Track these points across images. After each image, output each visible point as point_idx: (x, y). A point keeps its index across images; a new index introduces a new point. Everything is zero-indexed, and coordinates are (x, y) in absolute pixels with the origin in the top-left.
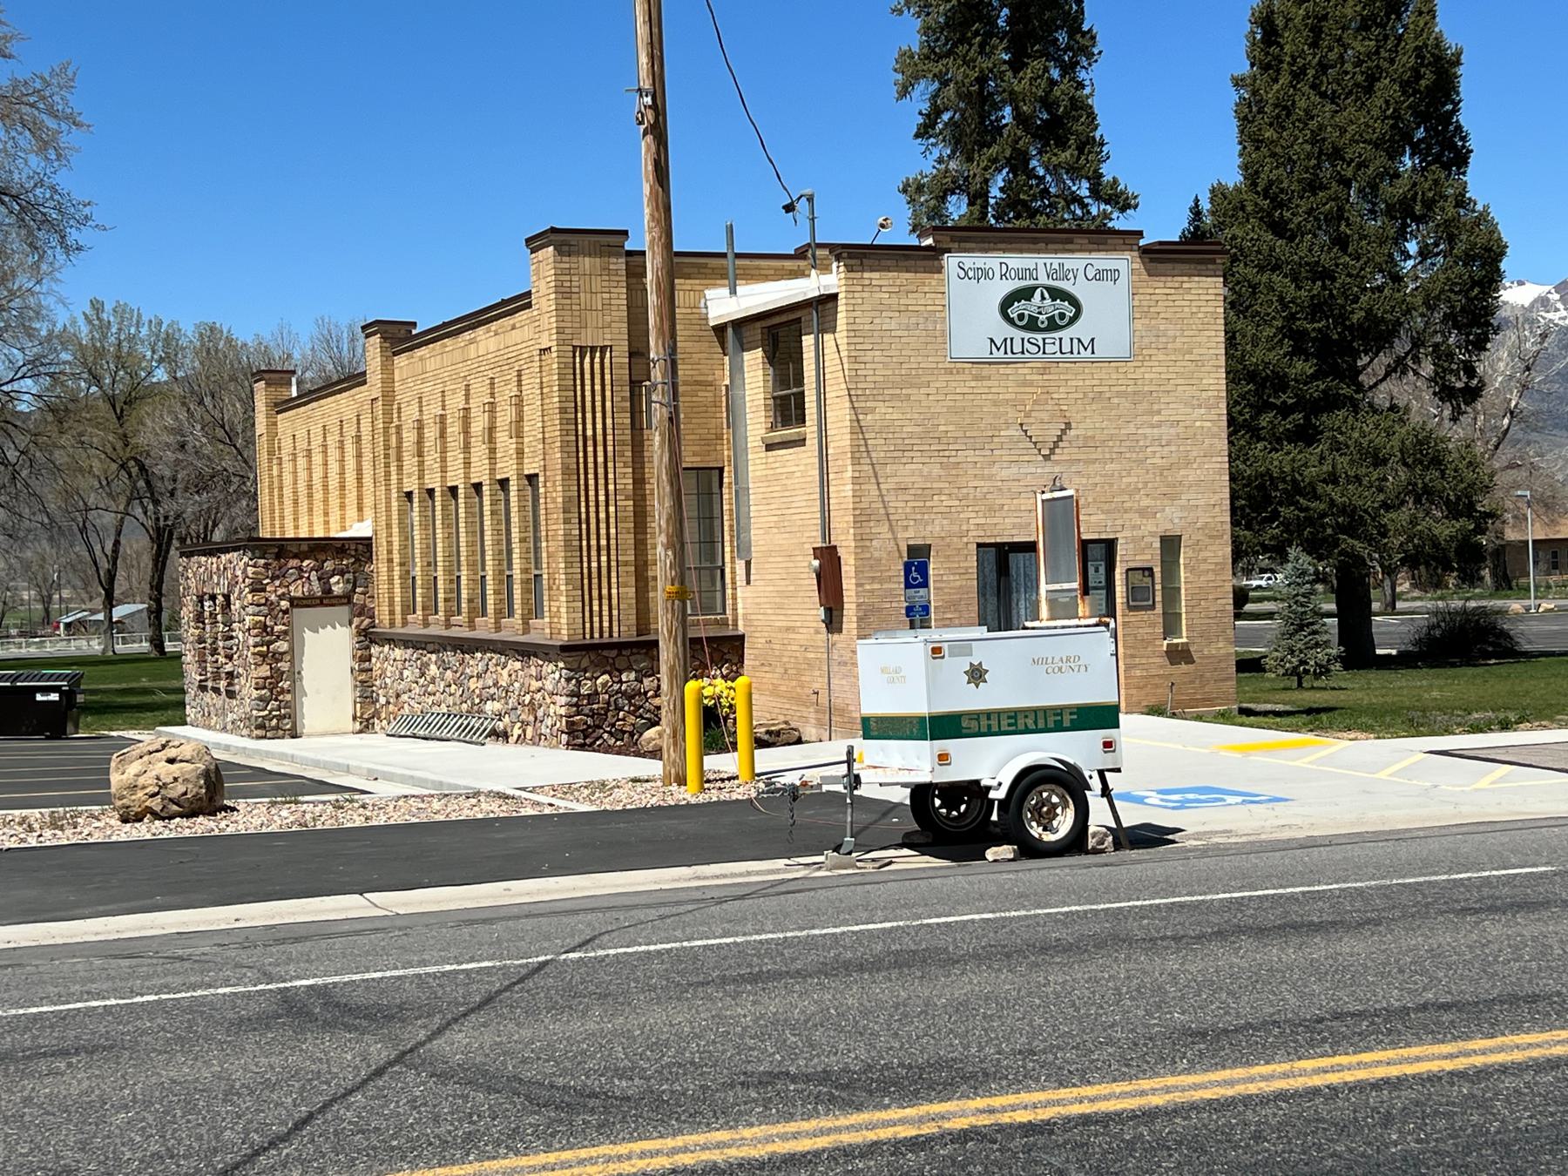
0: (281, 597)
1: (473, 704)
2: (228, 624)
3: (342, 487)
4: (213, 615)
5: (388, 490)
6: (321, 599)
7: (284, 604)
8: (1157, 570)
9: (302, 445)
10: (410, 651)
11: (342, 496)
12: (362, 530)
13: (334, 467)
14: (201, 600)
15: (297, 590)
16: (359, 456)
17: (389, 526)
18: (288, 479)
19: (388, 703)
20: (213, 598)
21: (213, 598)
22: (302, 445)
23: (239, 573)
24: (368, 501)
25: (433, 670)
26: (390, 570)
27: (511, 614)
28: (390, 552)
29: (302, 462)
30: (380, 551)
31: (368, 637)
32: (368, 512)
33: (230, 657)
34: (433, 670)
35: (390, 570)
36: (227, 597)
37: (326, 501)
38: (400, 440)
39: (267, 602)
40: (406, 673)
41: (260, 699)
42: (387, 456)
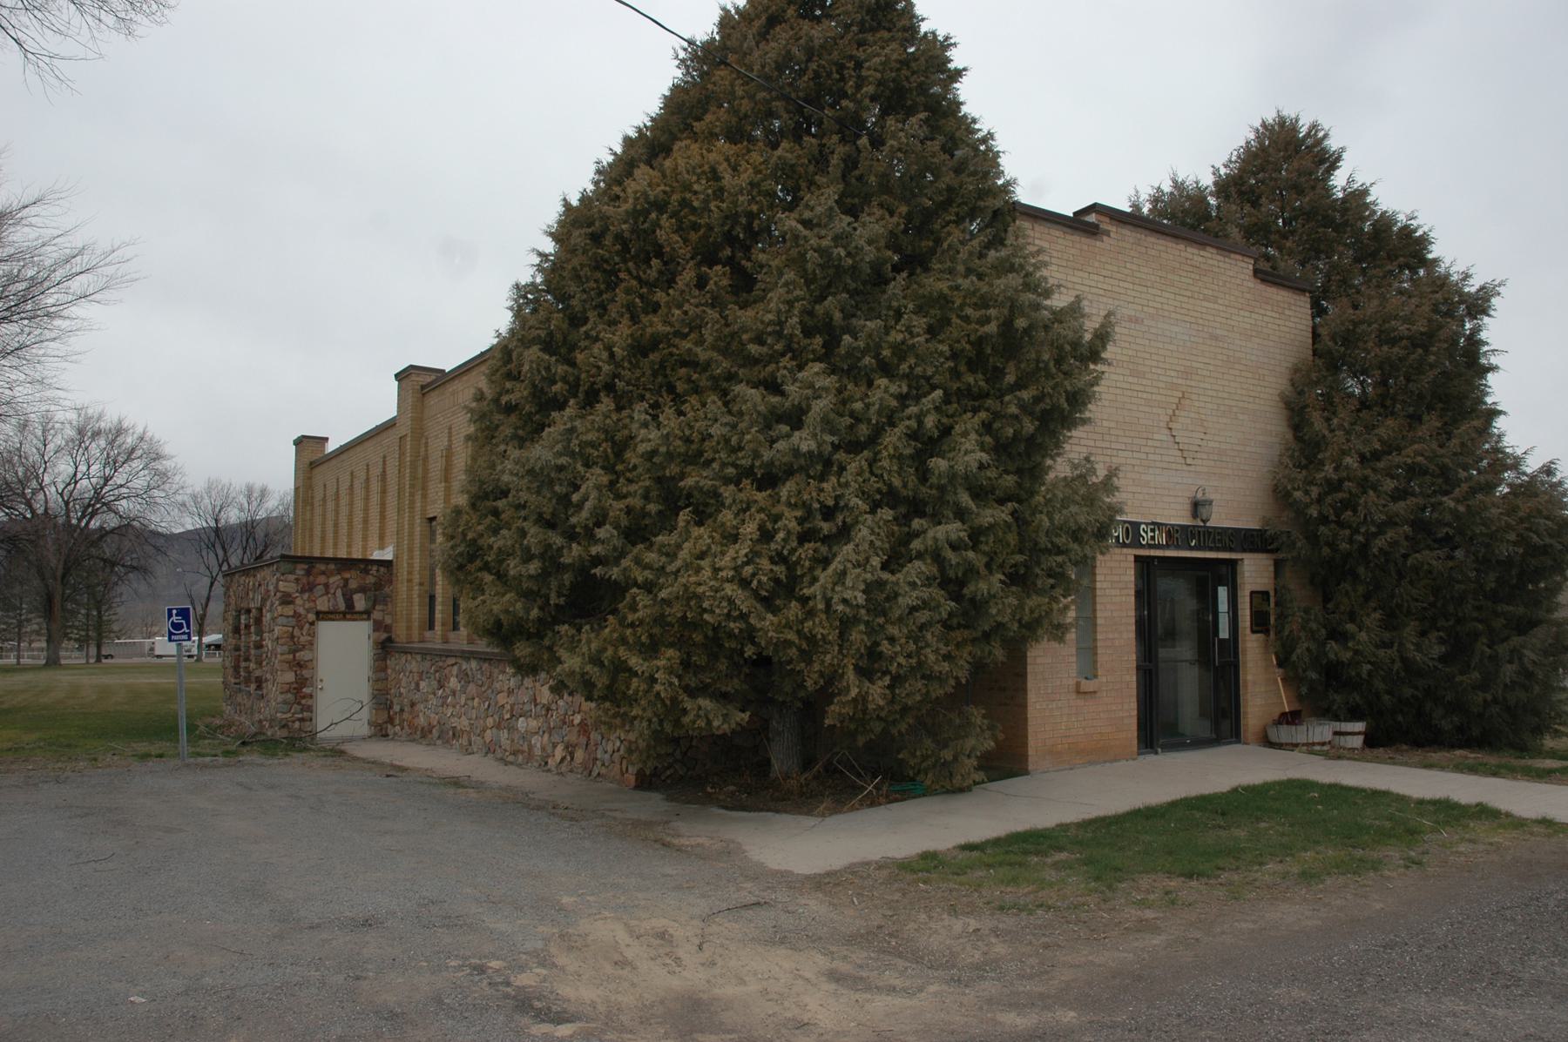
0: (308, 611)
1: (501, 718)
2: (260, 632)
3: (366, 521)
4: (247, 627)
5: (412, 518)
6: (344, 614)
7: (311, 617)
8: (1272, 593)
9: (331, 491)
10: (427, 664)
11: (365, 529)
12: (387, 554)
13: (359, 504)
14: (239, 612)
15: (323, 604)
16: (384, 492)
17: (411, 550)
18: (318, 519)
19: (402, 710)
20: (248, 611)
21: (248, 611)
22: (331, 491)
23: (271, 587)
24: (392, 526)
25: (453, 683)
26: (410, 589)
27: (431, 627)
28: (410, 573)
29: (331, 505)
30: (402, 573)
31: (385, 648)
32: (391, 539)
33: (260, 664)
34: (453, 683)
35: (410, 589)
36: (260, 610)
37: (350, 535)
38: (426, 471)
39: (296, 615)
40: (423, 684)
41: (285, 702)
42: (412, 486)
